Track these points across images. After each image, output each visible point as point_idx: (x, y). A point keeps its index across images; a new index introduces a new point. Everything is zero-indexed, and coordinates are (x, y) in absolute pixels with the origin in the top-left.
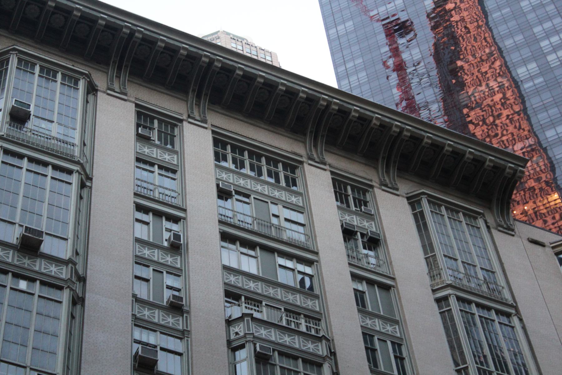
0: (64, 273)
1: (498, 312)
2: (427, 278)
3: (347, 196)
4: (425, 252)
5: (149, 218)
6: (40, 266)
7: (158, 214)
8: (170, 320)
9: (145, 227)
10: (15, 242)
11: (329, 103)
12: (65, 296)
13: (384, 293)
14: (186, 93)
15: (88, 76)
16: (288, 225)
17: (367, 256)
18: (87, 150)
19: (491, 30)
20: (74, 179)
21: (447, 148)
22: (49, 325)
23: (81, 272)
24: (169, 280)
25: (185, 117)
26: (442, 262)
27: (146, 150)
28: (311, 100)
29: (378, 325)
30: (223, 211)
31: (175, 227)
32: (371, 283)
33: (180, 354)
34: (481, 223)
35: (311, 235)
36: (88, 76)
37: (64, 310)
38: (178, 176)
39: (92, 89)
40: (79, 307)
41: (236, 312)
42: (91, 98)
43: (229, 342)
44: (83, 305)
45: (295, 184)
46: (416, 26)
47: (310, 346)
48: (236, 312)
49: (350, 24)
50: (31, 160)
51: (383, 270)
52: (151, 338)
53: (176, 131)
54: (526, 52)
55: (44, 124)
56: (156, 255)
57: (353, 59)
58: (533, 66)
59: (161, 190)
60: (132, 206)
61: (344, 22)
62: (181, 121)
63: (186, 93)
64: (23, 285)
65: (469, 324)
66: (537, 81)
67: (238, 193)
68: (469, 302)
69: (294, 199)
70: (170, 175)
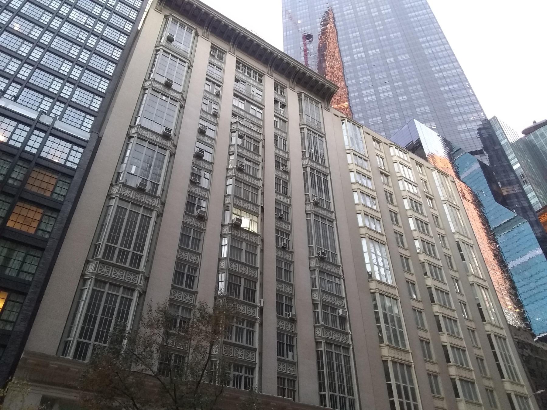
0: (179, 96)
1: (319, 135)
2: (299, 121)
3: (278, 89)
4: (300, 112)
5: (210, 84)
6: (171, 93)
7: (213, 83)
8: (212, 119)
9: (209, 86)
10: (163, 83)
11: (300, 69)
12: (178, 104)
13: (284, 123)
14: (229, 42)
15: (196, 29)
16: (257, 95)
17: (281, 110)
18: (192, 56)
19: (338, 42)
20: (186, 65)
21: (314, 78)
22: (171, 113)
23: (175, 143)
24: (214, 106)
25: (228, 51)
26: (305, 116)
27: (213, 60)
28: (271, 53)
29: (280, 133)
30: (235, 86)
31: (219, 88)
32: (280, 119)
33: (208, 179)
34: (320, 106)
35: (264, 100)
36: (196, 29)
37: (177, 109)
38: (222, 71)
39: (197, 35)
40: (182, 109)
41: (234, 120)
42: (196, 37)
43: (231, 130)
44: (184, 109)
45: (261, 82)
46: (314, 38)
47: (257, 136)
48: (234, 120)
49: (291, 32)
50: (172, 55)
51: (285, 116)
52: (206, 124)
53: (224, 55)
54: (348, 52)
55: (178, 44)
56: (211, 97)
57: (290, 45)
58: (405, 97)
59: (216, 75)
60: (205, 79)
61: (289, 31)
62: (226, 52)
63: (229, 42)
64: (164, 98)
65: (317, 226)
66: (349, 63)
67: (241, 81)
68: (311, 131)
69: (260, 87)
70: (220, 70)
